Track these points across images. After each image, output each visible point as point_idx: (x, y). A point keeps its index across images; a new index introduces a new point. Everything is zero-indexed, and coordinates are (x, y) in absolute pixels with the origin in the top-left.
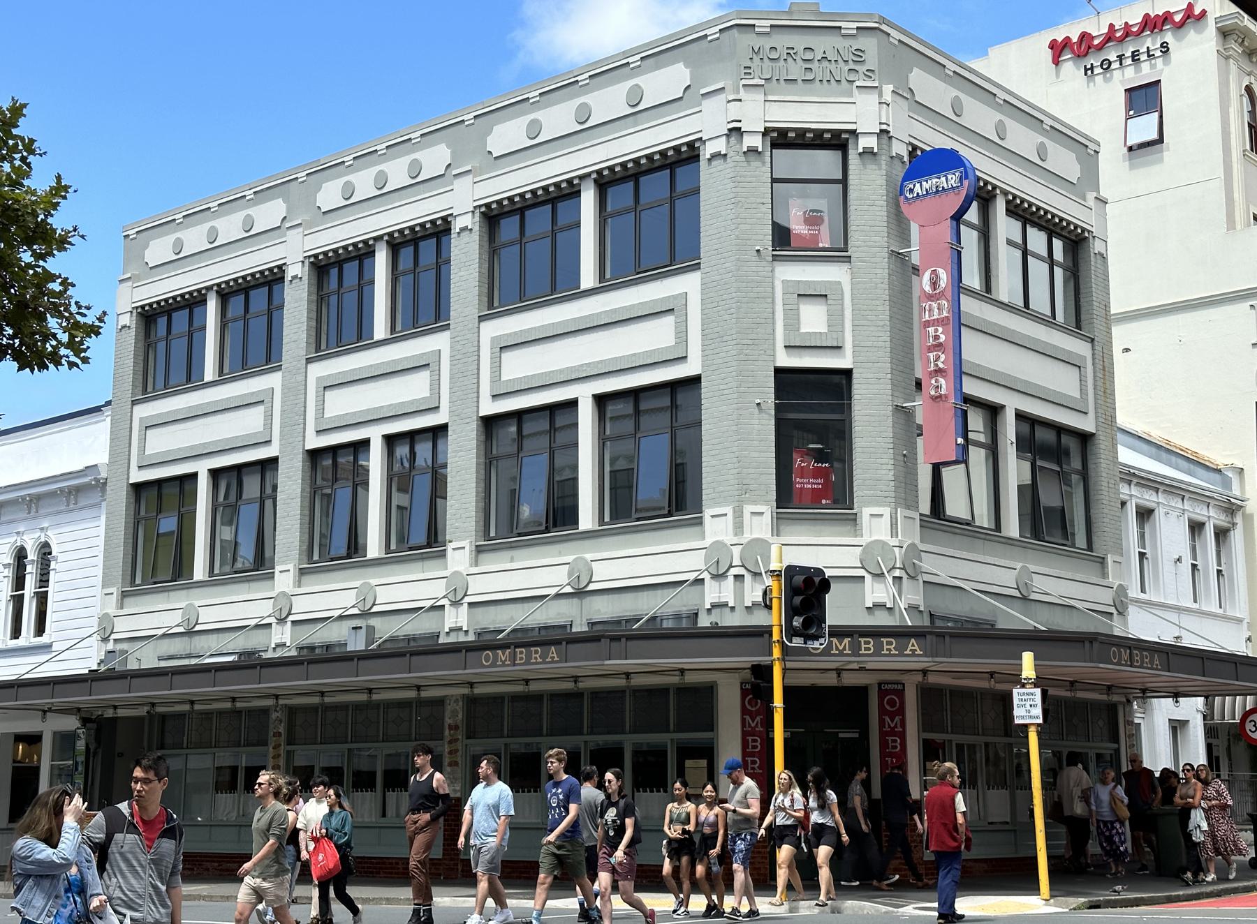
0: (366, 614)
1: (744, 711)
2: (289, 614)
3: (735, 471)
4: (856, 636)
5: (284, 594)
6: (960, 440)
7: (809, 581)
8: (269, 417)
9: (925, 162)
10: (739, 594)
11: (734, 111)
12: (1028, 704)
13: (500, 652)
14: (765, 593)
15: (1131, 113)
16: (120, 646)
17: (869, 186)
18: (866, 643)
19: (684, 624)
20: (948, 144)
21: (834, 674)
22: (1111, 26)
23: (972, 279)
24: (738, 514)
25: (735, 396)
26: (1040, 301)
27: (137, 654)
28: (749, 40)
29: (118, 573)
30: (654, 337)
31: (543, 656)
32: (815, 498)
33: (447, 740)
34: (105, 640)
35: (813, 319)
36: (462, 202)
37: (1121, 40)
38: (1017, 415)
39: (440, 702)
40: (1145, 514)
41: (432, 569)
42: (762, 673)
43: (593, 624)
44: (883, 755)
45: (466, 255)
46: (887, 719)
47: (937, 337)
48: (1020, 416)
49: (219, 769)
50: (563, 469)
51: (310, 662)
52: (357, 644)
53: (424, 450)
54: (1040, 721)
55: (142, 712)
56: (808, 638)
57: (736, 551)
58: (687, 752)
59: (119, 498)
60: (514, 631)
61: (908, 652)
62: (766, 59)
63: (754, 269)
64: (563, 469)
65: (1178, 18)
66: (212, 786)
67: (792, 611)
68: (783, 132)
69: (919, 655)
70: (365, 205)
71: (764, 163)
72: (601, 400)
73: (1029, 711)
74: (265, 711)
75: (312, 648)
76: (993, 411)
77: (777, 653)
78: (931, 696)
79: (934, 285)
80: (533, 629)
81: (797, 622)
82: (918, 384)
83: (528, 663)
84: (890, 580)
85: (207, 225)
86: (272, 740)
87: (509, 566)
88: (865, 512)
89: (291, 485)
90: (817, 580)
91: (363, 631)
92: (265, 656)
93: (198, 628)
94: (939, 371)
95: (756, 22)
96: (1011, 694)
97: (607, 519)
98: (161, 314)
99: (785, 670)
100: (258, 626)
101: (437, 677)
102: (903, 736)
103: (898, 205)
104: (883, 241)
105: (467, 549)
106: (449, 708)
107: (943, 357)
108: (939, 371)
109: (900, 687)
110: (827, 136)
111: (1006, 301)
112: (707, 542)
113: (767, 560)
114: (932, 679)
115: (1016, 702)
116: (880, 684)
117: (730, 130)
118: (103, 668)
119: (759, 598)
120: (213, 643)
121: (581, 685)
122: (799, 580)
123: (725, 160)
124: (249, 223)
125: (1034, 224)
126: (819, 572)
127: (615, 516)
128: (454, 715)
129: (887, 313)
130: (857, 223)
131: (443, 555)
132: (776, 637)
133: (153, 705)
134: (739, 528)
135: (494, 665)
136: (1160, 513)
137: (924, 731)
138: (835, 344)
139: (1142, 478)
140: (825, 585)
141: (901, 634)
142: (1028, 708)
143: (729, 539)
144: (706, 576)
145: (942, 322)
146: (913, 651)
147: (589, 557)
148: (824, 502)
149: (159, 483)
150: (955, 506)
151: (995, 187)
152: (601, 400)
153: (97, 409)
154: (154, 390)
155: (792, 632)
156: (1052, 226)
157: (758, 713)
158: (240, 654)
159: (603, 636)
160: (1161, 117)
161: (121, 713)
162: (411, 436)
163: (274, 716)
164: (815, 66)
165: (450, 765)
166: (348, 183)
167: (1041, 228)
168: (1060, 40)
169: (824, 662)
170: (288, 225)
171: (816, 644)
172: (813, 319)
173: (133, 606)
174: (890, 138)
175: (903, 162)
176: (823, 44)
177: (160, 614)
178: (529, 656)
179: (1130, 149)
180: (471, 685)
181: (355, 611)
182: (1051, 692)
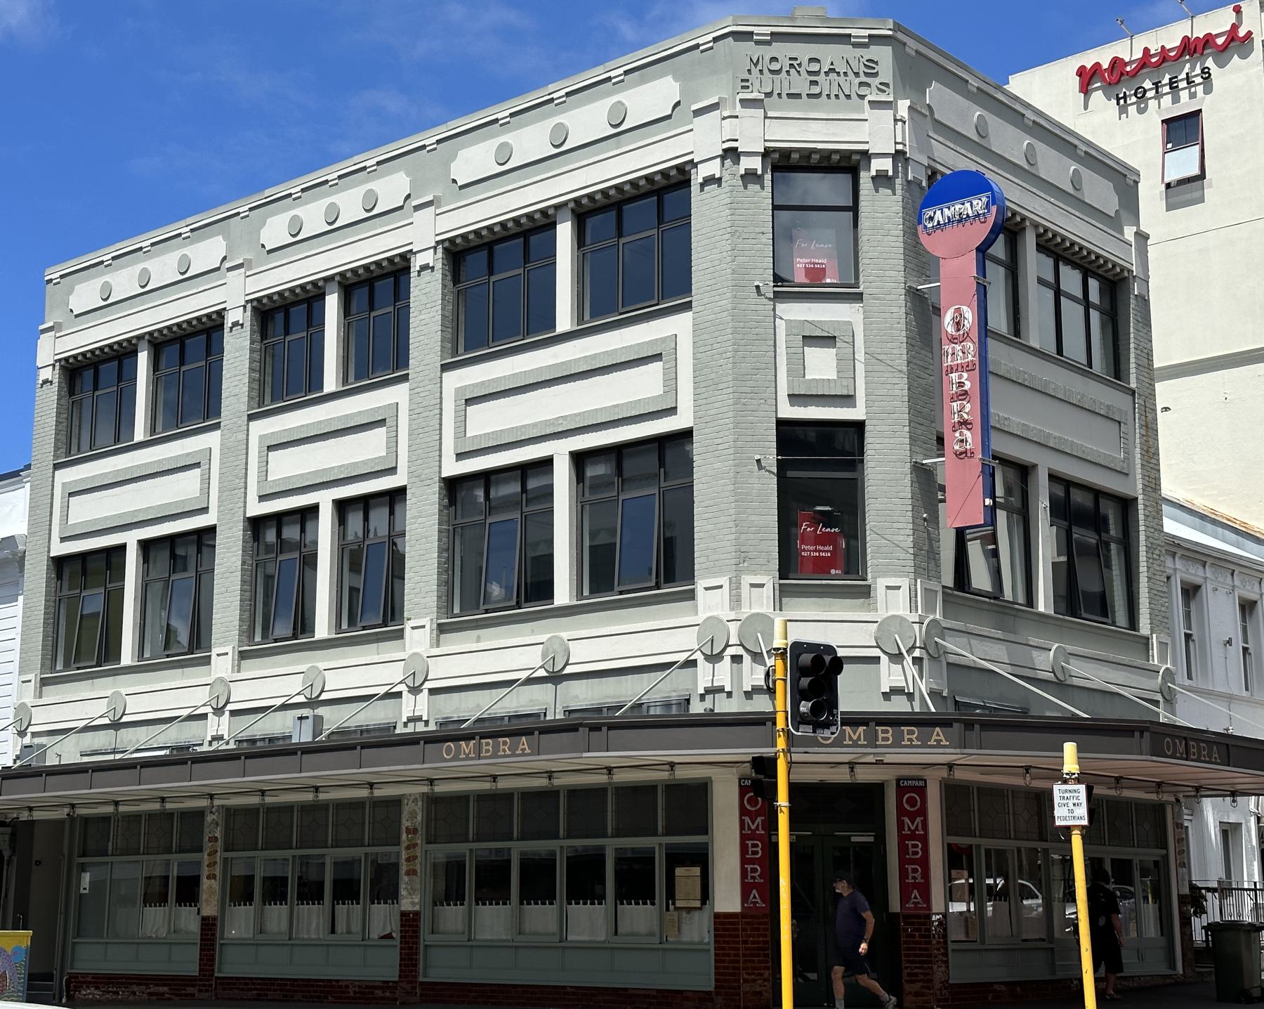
0: (313, 703)
1: (743, 811)
2: (227, 702)
3: (733, 537)
4: (872, 724)
5: (221, 680)
6: (988, 502)
7: (818, 660)
8: (206, 480)
9: (942, 188)
10: (737, 677)
11: (730, 129)
12: (1071, 802)
13: (463, 743)
14: (767, 674)
15: (1170, 146)
16: (37, 741)
17: (882, 212)
18: (883, 732)
19: (674, 711)
20: (973, 168)
21: (846, 769)
22: (1146, 50)
23: (999, 320)
24: (735, 585)
25: (731, 451)
26: (1074, 347)
27: (56, 749)
28: (748, 47)
29: (37, 659)
30: (643, 385)
31: (513, 748)
32: (821, 567)
33: (404, 845)
34: (22, 734)
35: (821, 366)
36: (422, 236)
37: (1158, 65)
38: (1050, 475)
39: (396, 802)
40: (1191, 592)
41: (388, 651)
42: (765, 766)
43: (570, 712)
44: (903, 862)
45: (427, 300)
46: (907, 820)
47: (961, 384)
48: (1054, 477)
49: (148, 879)
50: (538, 544)
51: (250, 756)
52: (304, 736)
53: (379, 517)
54: (1085, 822)
55: (62, 814)
56: (818, 726)
57: (734, 628)
58: (677, 858)
59: (36, 576)
60: (479, 720)
61: (932, 742)
62: (766, 71)
63: (753, 307)
64: (538, 544)
65: (1220, 41)
66: (140, 898)
67: (799, 695)
68: (786, 153)
69: (945, 747)
70: (312, 231)
71: (763, 188)
72: (580, 459)
73: (1072, 811)
74: (199, 814)
75: (253, 741)
76: (1024, 471)
77: (781, 743)
78: (955, 793)
79: (958, 325)
80: (502, 718)
81: (805, 707)
82: (940, 440)
83: (495, 755)
84: (909, 660)
85: (138, 268)
86: (208, 847)
87: (474, 647)
88: (880, 585)
89: (229, 559)
90: (827, 658)
91: (310, 721)
92: (199, 749)
93: (125, 719)
94: (964, 423)
95: (756, 30)
96: (1049, 794)
97: (586, 593)
98: (86, 367)
99: (790, 764)
100: (191, 718)
101: (397, 777)
102: (924, 840)
103: (915, 234)
104: (900, 276)
105: (428, 627)
106: (406, 810)
107: (968, 407)
108: (964, 423)
109: (921, 783)
110: (836, 157)
111: (1037, 347)
112: (699, 619)
113: (769, 636)
114: (959, 775)
115: (1057, 800)
116: (898, 781)
117: (725, 151)
118: (19, 763)
119: (759, 680)
120: (139, 737)
121: (556, 782)
122: (806, 658)
123: (720, 186)
124: (185, 264)
125: (1069, 262)
126: (830, 649)
127: (594, 590)
128: (412, 816)
129: (905, 357)
130: (870, 255)
131: (399, 635)
132: (780, 724)
133: (73, 806)
134: (736, 601)
135: (455, 758)
136: (1207, 589)
137: (948, 834)
138: (845, 392)
139: (1188, 549)
140: (838, 664)
141: (923, 722)
142: (1070, 807)
143: (725, 613)
144: (698, 656)
145: (967, 368)
146: (939, 741)
147: (565, 635)
148: (833, 571)
149: (83, 556)
150: (980, 578)
151: (1024, 219)
152: (580, 459)
153: (16, 474)
154: (79, 451)
155: (798, 719)
156: (1088, 265)
157: (758, 813)
158: (172, 748)
159: (581, 725)
160: (1202, 150)
161: (37, 815)
162: (365, 502)
163: (209, 818)
164: (821, 78)
165: (408, 873)
166: (295, 218)
167: (1075, 265)
168: (1089, 66)
169: (832, 759)
170: (227, 265)
171: (827, 733)
172: (821, 366)
173: (54, 694)
174: (907, 160)
175: (922, 188)
176: (830, 54)
177: (84, 702)
178: (496, 748)
179: (1168, 186)
180: (431, 782)
181: (301, 699)
182: (1097, 790)
